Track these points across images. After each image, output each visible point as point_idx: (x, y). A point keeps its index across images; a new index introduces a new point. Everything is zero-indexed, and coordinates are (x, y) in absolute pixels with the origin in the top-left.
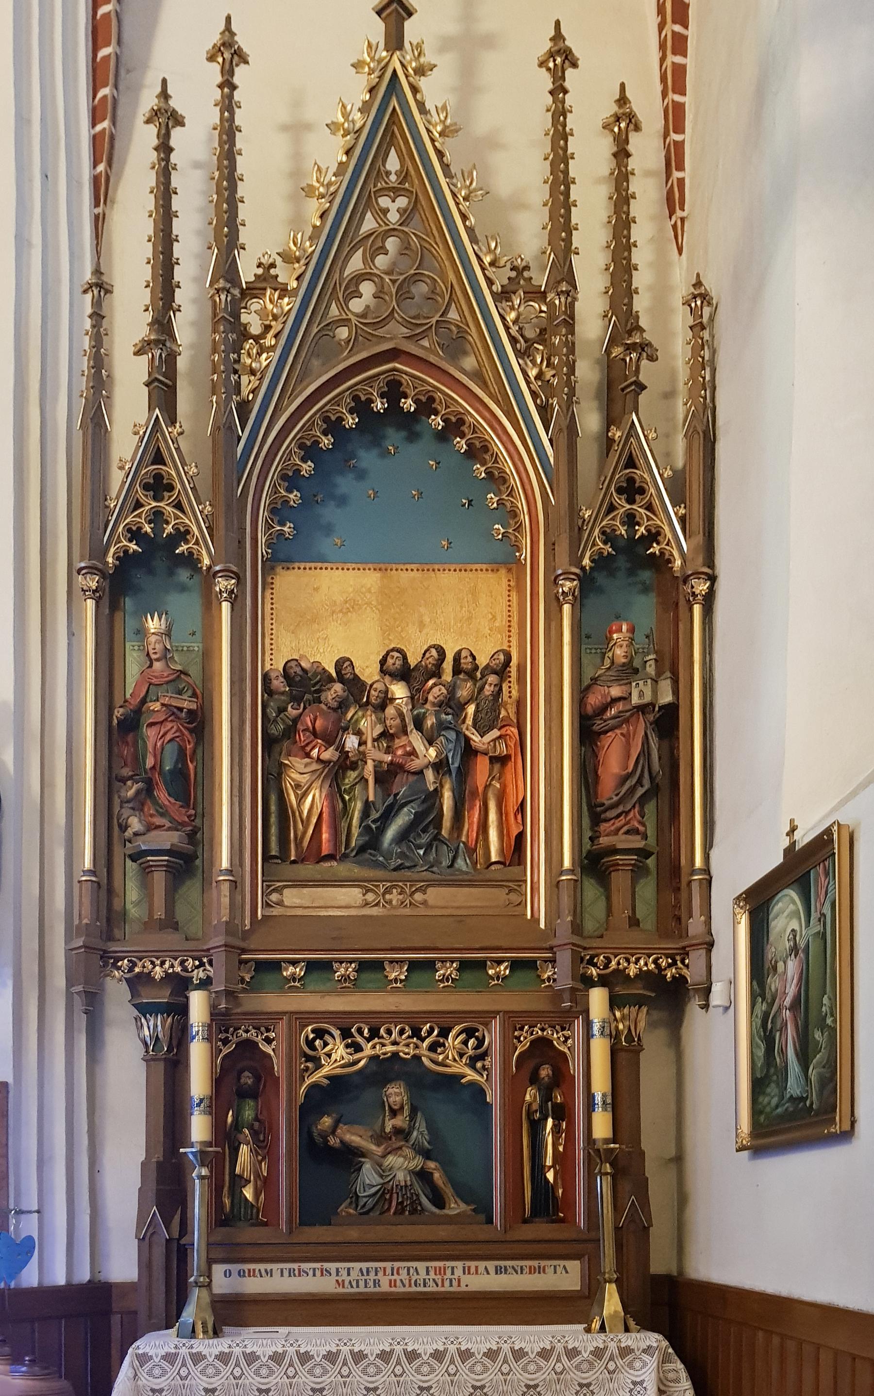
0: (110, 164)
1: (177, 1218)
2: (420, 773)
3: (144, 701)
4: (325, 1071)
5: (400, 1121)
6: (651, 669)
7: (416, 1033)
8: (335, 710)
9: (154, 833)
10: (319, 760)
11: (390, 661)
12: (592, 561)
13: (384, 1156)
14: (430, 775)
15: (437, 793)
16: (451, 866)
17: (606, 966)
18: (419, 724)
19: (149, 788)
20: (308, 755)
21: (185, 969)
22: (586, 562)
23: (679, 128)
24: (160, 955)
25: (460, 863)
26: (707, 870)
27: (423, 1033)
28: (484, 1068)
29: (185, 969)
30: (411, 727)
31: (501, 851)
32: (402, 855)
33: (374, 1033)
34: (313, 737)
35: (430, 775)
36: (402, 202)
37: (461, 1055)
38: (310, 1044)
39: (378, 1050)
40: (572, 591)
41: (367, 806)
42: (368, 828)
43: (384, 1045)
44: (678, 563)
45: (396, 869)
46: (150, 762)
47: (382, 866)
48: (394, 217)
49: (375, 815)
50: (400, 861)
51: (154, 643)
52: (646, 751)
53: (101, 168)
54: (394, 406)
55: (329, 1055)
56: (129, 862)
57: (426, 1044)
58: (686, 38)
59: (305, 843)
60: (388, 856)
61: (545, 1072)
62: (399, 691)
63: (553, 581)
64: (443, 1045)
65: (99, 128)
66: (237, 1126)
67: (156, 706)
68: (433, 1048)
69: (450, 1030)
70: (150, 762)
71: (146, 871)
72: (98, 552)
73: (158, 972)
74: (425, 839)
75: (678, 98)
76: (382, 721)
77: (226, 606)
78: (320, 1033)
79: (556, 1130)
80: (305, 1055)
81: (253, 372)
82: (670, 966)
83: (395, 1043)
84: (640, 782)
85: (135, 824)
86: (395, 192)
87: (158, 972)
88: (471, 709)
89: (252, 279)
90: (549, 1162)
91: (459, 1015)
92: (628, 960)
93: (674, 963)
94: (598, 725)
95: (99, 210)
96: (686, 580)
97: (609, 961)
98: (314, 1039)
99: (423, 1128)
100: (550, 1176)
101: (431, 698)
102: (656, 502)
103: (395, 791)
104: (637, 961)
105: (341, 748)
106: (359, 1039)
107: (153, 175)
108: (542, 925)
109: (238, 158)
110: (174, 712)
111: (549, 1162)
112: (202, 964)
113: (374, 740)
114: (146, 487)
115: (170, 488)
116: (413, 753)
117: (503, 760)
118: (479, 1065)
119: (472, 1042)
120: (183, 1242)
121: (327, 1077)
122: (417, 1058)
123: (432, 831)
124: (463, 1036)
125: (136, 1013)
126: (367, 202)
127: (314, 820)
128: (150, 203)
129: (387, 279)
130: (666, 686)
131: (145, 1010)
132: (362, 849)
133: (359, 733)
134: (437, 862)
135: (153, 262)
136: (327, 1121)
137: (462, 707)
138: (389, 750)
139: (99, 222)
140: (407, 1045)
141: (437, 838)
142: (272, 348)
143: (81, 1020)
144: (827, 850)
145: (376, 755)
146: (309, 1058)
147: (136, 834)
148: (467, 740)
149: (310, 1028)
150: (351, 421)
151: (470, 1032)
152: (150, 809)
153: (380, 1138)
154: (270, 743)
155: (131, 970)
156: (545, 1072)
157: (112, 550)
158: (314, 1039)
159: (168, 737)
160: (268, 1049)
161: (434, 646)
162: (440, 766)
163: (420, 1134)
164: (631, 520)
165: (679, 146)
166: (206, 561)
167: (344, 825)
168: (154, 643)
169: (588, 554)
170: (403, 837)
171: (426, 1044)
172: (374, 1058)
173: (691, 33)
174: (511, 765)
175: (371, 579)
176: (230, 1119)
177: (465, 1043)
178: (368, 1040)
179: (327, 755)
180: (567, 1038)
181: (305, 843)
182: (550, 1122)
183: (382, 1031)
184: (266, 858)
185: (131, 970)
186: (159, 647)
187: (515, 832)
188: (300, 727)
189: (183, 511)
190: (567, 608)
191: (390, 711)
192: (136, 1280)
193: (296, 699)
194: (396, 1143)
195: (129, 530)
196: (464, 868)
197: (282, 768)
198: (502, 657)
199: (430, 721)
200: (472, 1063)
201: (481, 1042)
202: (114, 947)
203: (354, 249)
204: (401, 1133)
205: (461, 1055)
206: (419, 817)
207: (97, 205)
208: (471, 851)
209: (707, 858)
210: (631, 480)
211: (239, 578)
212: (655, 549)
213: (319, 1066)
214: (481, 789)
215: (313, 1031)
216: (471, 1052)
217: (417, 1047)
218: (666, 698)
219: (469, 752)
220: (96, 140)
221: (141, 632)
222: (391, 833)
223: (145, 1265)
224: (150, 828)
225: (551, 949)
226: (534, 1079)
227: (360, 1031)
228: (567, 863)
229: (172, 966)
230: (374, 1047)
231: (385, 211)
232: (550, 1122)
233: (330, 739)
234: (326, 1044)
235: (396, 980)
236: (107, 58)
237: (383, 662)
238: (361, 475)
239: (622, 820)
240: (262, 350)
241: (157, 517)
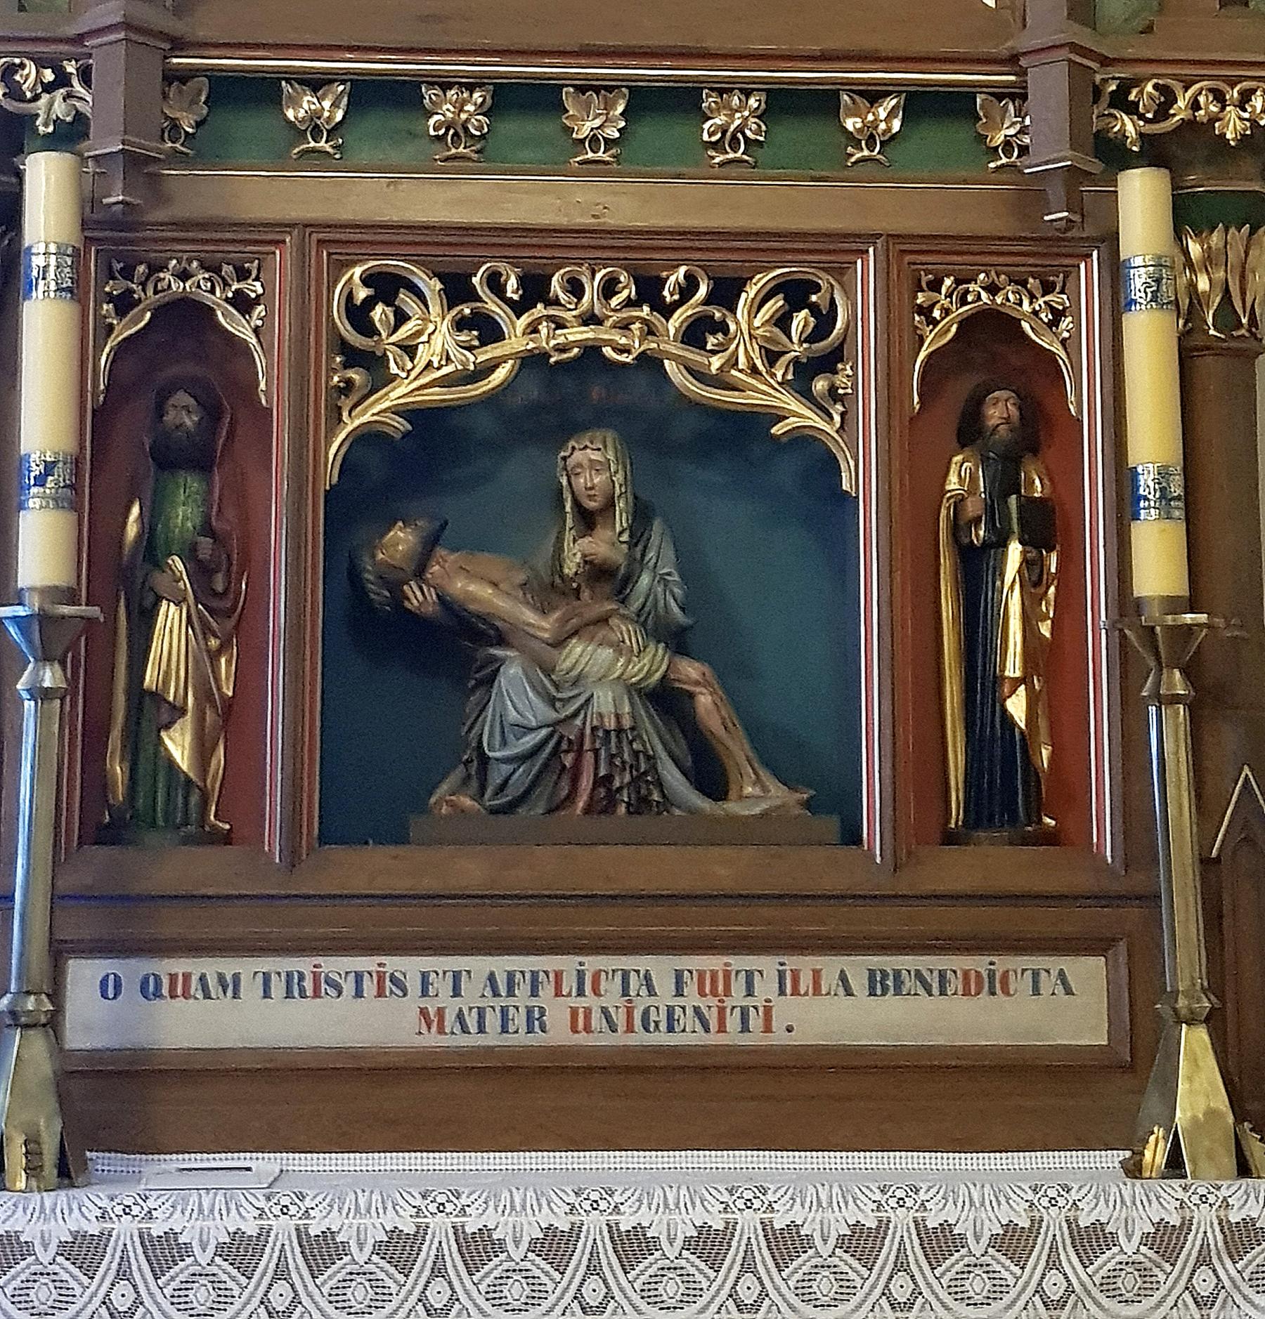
4: (397, 394)
13: (559, 643)
17: (1163, 112)
37: (772, 358)
38: (359, 315)
39: (546, 339)
43: (560, 324)
57: (675, 323)
68: (694, 334)
79: (1033, 575)
80: (344, 347)
83: (590, 319)
90: (1013, 667)
92: (1219, 97)
97: (1169, 97)
98: (369, 303)
106: (493, 306)
111: (1013, 667)
112: (62, 80)
118: (820, 385)
119: (801, 319)
124: (776, 304)
146: (354, 357)
149: (358, 271)
158: (369, 303)
160: (241, 328)
171: (675, 323)
172: (532, 361)
176: (132, 530)
177: (783, 322)
178: (519, 309)
180: (1058, 315)
182: (1015, 551)
183: (556, 286)
194: (594, 604)
201: (825, 320)
205: (772, 358)
215: (366, 281)
216: (797, 350)
217: (650, 331)
230: (533, 329)
235: (594, 140)
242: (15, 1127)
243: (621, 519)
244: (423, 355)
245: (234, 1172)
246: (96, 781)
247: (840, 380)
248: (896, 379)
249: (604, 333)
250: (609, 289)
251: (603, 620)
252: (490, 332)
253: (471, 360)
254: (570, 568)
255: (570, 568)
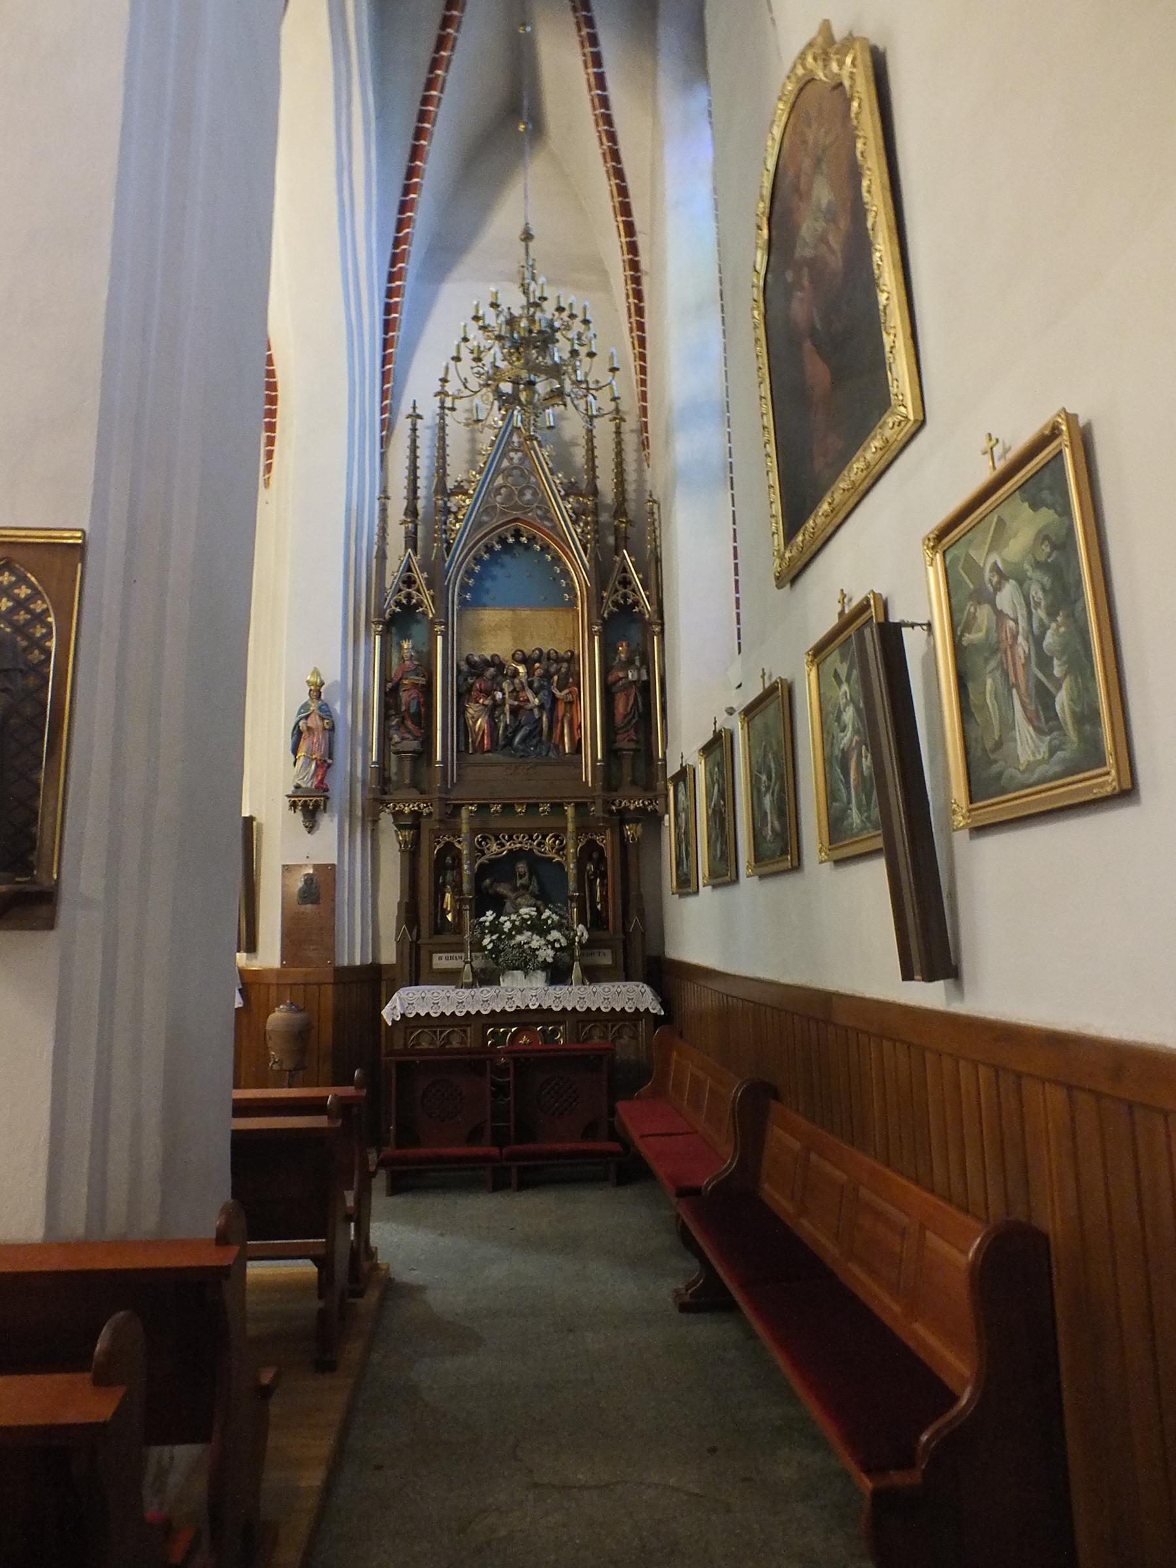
0: (388, 430)
1: (415, 930)
2: (531, 710)
3: (401, 679)
4: (487, 856)
5: (524, 881)
6: (638, 663)
7: (531, 838)
8: (491, 680)
9: (405, 742)
10: (483, 704)
11: (517, 656)
12: (608, 614)
13: (516, 899)
14: (536, 711)
15: (541, 718)
16: (547, 754)
17: (620, 805)
18: (530, 685)
19: (402, 722)
20: (478, 702)
21: (419, 808)
22: (605, 615)
23: (645, 416)
24: (408, 801)
25: (551, 754)
26: (664, 759)
27: (534, 838)
28: (563, 854)
29: (419, 808)
30: (527, 688)
31: (570, 748)
32: (523, 750)
33: (510, 838)
34: (532, 300)
35: (536, 711)
36: (520, 454)
37: (553, 848)
38: (479, 843)
39: (513, 846)
40: (599, 630)
41: (506, 727)
42: (507, 736)
43: (515, 844)
44: (647, 616)
45: (522, 757)
46: (403, 708)
47: (512, 755)
48: (516, 461)
49: (510, 730)
50: (522, 754)
51: (406, 654)
52: (636, 700)
53: (384, 433)
54: (518, 542)
55: (488, 849)
56: (392, 754)
57: (535, 843)
58: (645, 380)
59: (477, 745)
60: (516, 750)
61: (595, 855)
62: (522, 669)
63: (590, 625)
64: (544, 844)
65: (384, 416)
66: (444, 884)
67: (406, 682)
68: (539, 845)
69: (547, 836)
70: (403, 708)
71: (400, 760)
72: (380, 612)
73: (407, 810)
74: (534, 742)
75: (644, 404)
76: (513, 683)
77: (439, 638)
78: (484, 838)
79: (602, 884)
80: (477, 849)
81: (453, 530)
82: (649, 804)
83: (520, 843)
84: (634, 717)
85: (396, 738)
86: (516, 451)
87: (407, 810)
88: (556, 678)
89: (452, 487)
90: (598, 900)
91: (551, 829)
92: (630, 803)
93: (652, 803)
94: (614, 689)
95: (383, 450)
96: (651, 624)
97: (621, 802)
98: (481, 842)
99: (535, 884)
100: (599, 907)
101: (536, 673)
102: (636, 589)
103: (519, 718)
104: (634, 802)
105: (494, 698)
106: (503, 841)
107: (408, 451)
108: (590, 785)
109: (447, 458)
110: (415, 685)
111: (598, 900)
112: (428, 806)
113: (509, 693)
114: (404, 582)
115: (415, 582)
116: (528, 700)
117: (571, 703)
118: (561, 853)
119: (557, 842)
120: (419, 942)
121: (489, 860)
122: (531, 850)
123: (538, 738)
124: (553, 839)
125: (396, 829)
126: (504, 455)
127: (481, 733)
128: (408, 452)
129: (513, 488)
130: (644, 671)
131: (401, 827)
132: (504, 746)
133: (502, 690)
134: (540, 754)
135: (408, 478)
136: (488, 881)
137: (552, 677)
138: (516, 699)
139: (383, 455)
140: (526, 844)
141: (540, 741)
142: (461, 520)
143: (369, 827)
144: (775, 694)
145: (509, 702)
146: (479, 851)
147: (396, 743)
148: (554, 694)
150: (498, 547)
151: (556, 837)
152: (402, 729)
153: (515, 889)
154: (459, 695)
155: (394, 808)
156: (595, 855)
157: (388, 611)
158: (481, 842)
159: (412, 696)
160: (459, 846)
161: (536, 649)
162: (541, 707)
163: (534, 887)
164: (625, 597)
165: (646, 423)
166: (431, 616)
167: (495, 734)
168: (406, 654)
169: (606, 612)
170: (523, 740)
171: (535, 843)
172: (510, 851)
173: (648, 378)
174: (574, 706)
175: (507, 615)
176: (441, 881)
177: (554, 842)
178: (508, 841)
179: (486, 702)
180: (603, 839)
181: (477, 745)
182: (598, 880)
183: (514, 837)
184: (458, 751)
185: (394, 808)
186: (408, 655)
187: (577, 738)
188: (474, 688)
189: (421, 594)
190: (596, 638)
191: (517, 681)
192: (395, 962)
193: (472, 675)
194: (522, 892)
195: (396, 602)
196: (553, 756)
197: (465, 709)
198: (569, 654)
199: (536, 685)
200: (557, 853)
201: (561, 842)
202: (386, 797)
203: (499, 475)
204: (525, 887)
205: (553, 848)
206: (531, 732)
207: (382, 447)
208: (557, 747)
209: (664, 753)
210: (625, 578)
211: (446, 624)
212: (636, 609)
213: (484, 854)
214: (560, 718)
215: (481, 837)
216: (557, 847)
217: (531, 844)
218: (645, 678)
219: (555, 700)
220: (383, 421)
221: (401, 647)
222: (517, 739)
223: (400, 954)
224: (403, 739)
225: (593, 797)
226: (590, 859)
227: (504, 837)
228: (599, 756)
229: (413, 807)
230: (510, 845)
231: (512, 459)
232: (598, 880)
233: (488, 693)
234: (487, 844)
235: (520, 812)
236: (388, 389)
237: (513, 655)
238: (503, 566)
239: (626, 734)
240: (458, 520)
241: (409, 597)
242: (397, 815)
243: (527, 877)
244: (491, 850)
245: (921, 408)
246: (436, 922)
247: (565, 852)
248: (665, 736)
249: (523, 845)
250: (524, 837)
251: (523, 895)
252: (503, 845)
253: (500, 850)
254: (518, 885)
255: (518, 885)
